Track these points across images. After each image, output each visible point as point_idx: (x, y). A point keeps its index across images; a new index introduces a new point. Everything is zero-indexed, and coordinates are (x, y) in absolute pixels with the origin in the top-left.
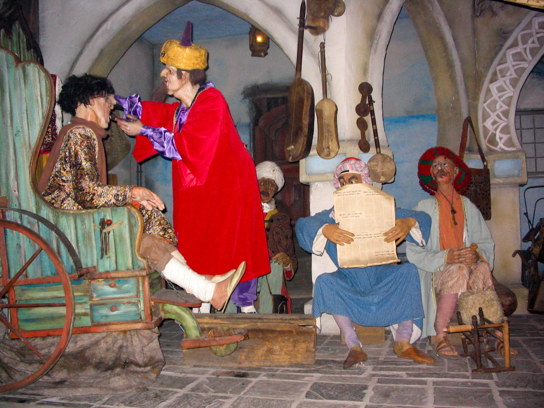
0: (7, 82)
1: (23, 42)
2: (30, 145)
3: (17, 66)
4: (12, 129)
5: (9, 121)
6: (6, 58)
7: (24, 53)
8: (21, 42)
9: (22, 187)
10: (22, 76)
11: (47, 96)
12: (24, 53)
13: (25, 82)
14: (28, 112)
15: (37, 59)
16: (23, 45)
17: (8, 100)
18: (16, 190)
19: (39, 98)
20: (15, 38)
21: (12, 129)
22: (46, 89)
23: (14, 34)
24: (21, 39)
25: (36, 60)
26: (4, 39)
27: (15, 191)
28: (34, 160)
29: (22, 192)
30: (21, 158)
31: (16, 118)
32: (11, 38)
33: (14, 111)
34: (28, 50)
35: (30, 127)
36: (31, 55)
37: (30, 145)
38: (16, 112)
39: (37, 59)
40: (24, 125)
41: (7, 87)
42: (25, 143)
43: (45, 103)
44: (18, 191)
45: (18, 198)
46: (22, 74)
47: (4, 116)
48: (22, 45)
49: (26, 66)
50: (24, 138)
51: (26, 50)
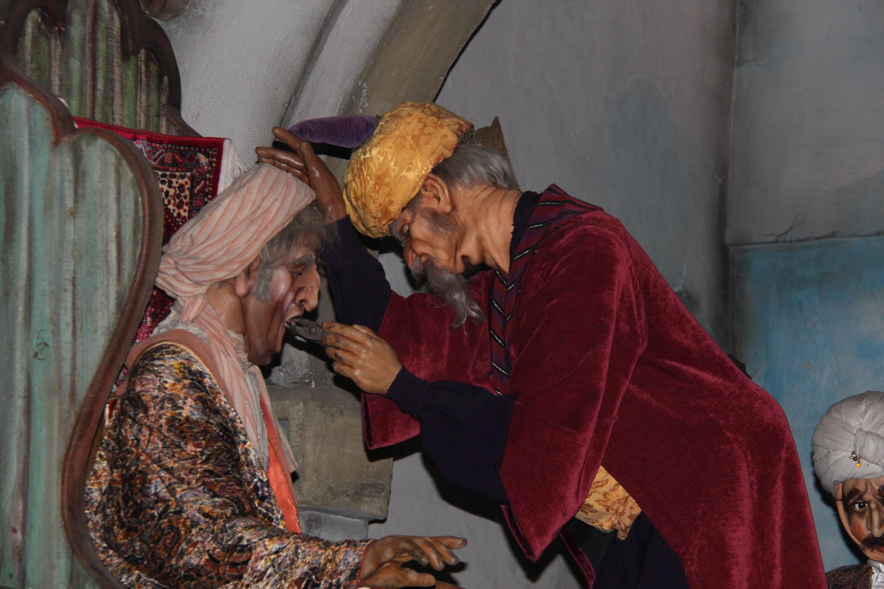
0: (26, 192)
1: (108, 35)
2: (73, 394)
3: (56, 143)
4: (28, 339)
5: (21, 309)
6: (29, 113)
7: (109, 70)
8: (100, 36)
9: (37, 520)
10: (70, 176)
11: (135, 242)
12: (109, 70)
13: (76, 194)
14: (79, 288)
15: (160, 81)
16: (108, 45)
17: (24, 245)
18: (19, 528)
19: (113, 247)
20: (77, 30)
21: (28, 339)
22: (136, 220)
23: (76, 18)
24: (102, 25)
25: (153, 83)
26: (35, 39)
27: (15, 531)
28: (81, 438)
29: (36, 536)
30: (45, 430)
31: (42, 308)
32: (64, 36)
33: (37, 280)
34: (125, 56)
35: (78, 333)
36: (138, 68)
37: (73, 394)
38: (42, 284)
39: (160, 81)
40: (63, 326)
41: (25, 204)
42: (60, 382)
43: (127, 265)
44: (24, 533)
45: (21, 554)
46: (71, 169)
47: (7, 294)
48: (102, 46)
49: (84, 146)
50: (59, 368)
51: (117, 60)
